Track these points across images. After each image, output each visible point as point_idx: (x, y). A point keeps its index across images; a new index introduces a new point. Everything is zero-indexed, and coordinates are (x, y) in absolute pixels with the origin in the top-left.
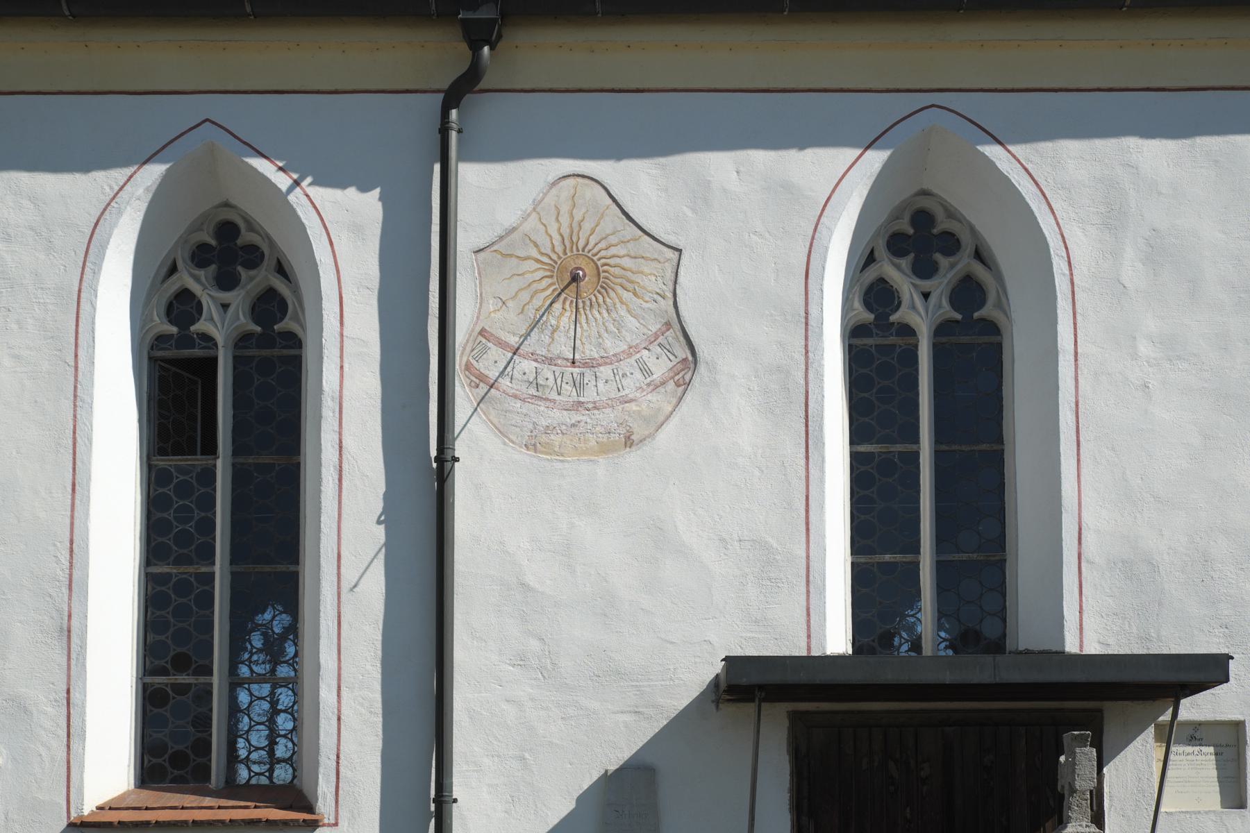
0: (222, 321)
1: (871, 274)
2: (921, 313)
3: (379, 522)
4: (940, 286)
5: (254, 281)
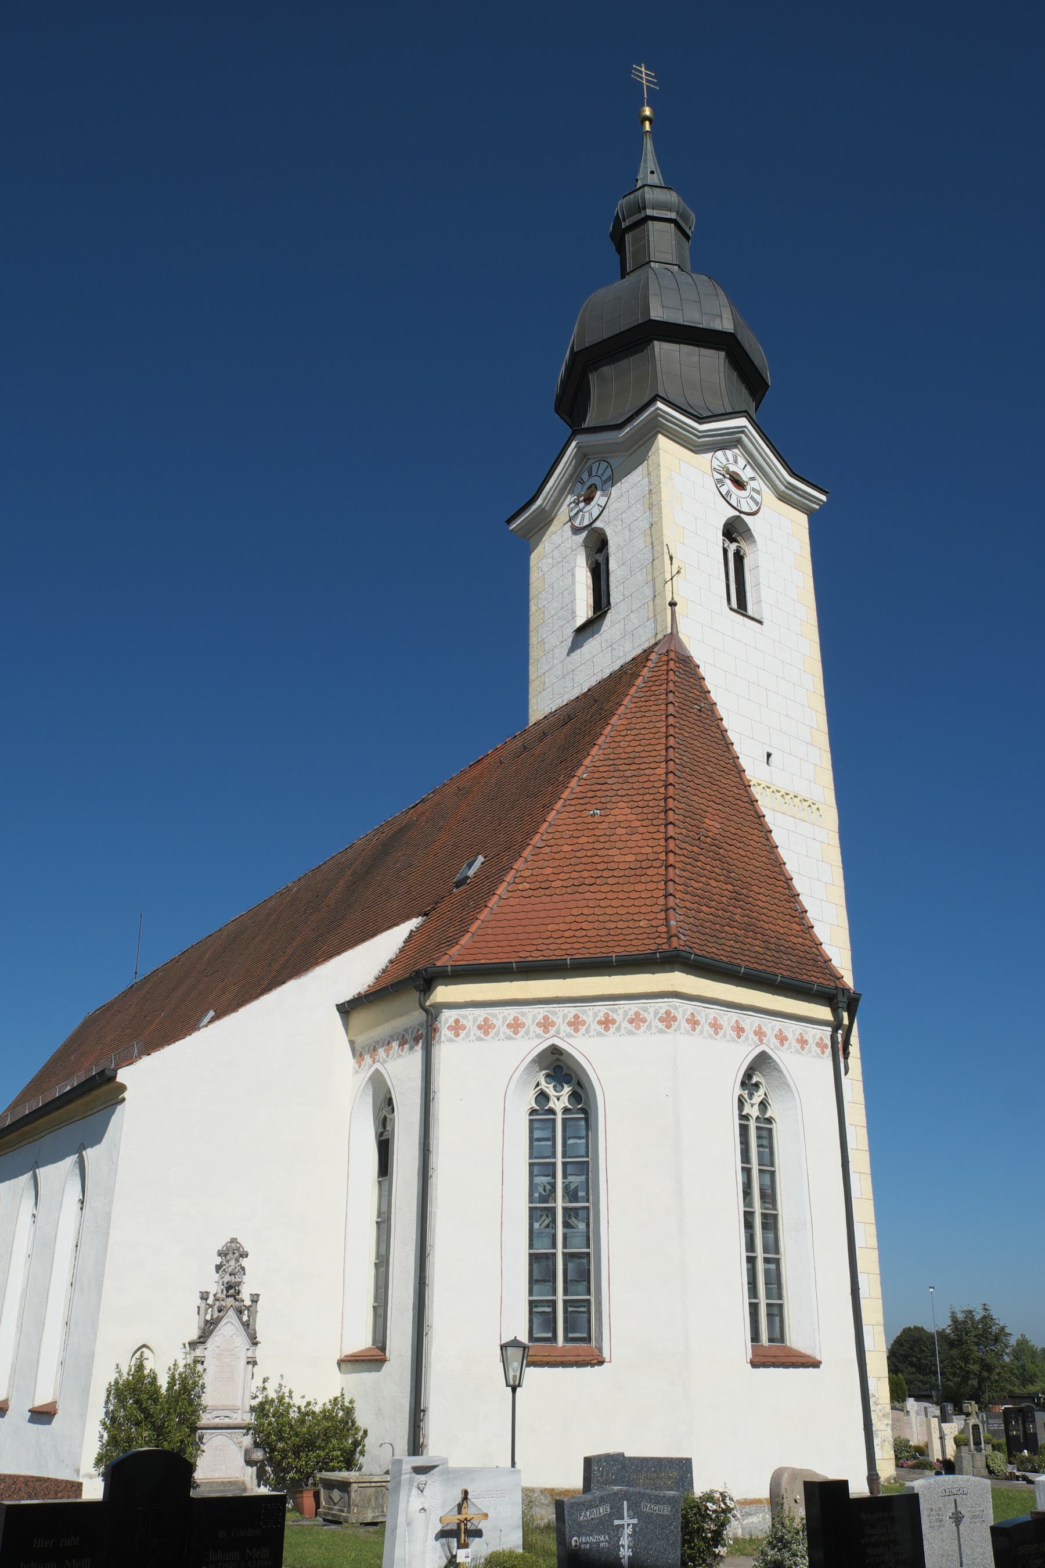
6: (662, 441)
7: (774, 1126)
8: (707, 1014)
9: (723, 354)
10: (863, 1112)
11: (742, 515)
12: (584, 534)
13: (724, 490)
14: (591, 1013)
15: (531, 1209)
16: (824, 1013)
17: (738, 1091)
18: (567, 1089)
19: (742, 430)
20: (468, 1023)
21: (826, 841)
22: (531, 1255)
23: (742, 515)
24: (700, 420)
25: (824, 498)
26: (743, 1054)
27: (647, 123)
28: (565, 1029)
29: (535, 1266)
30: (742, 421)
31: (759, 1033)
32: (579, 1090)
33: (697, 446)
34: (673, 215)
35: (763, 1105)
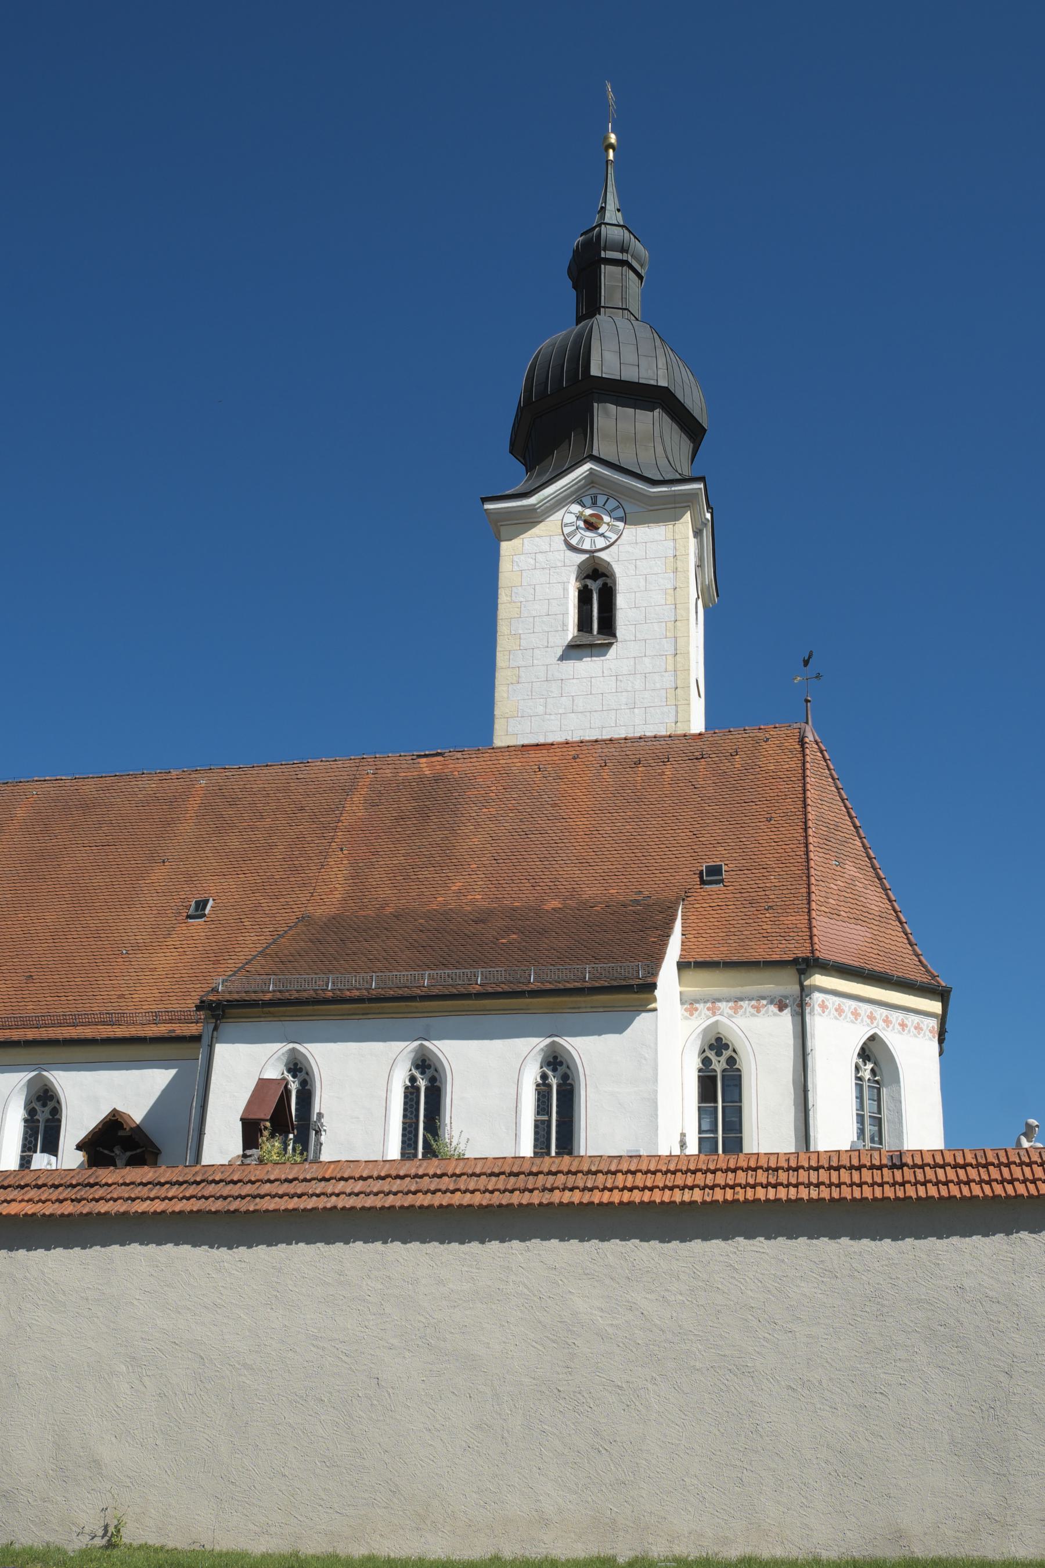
0: (719, 1065)
1: (704, 1055)
2: (422, 1084)
3: (79, 1147)
4: (723, 1059)
5: (726, 1054)
8: (913, 1019)
12: (584, 557)
17: (855, 1059)
18: (870, 1066)
28: (882, 1024)
31: (872, 1018)
32: (876, 1069)
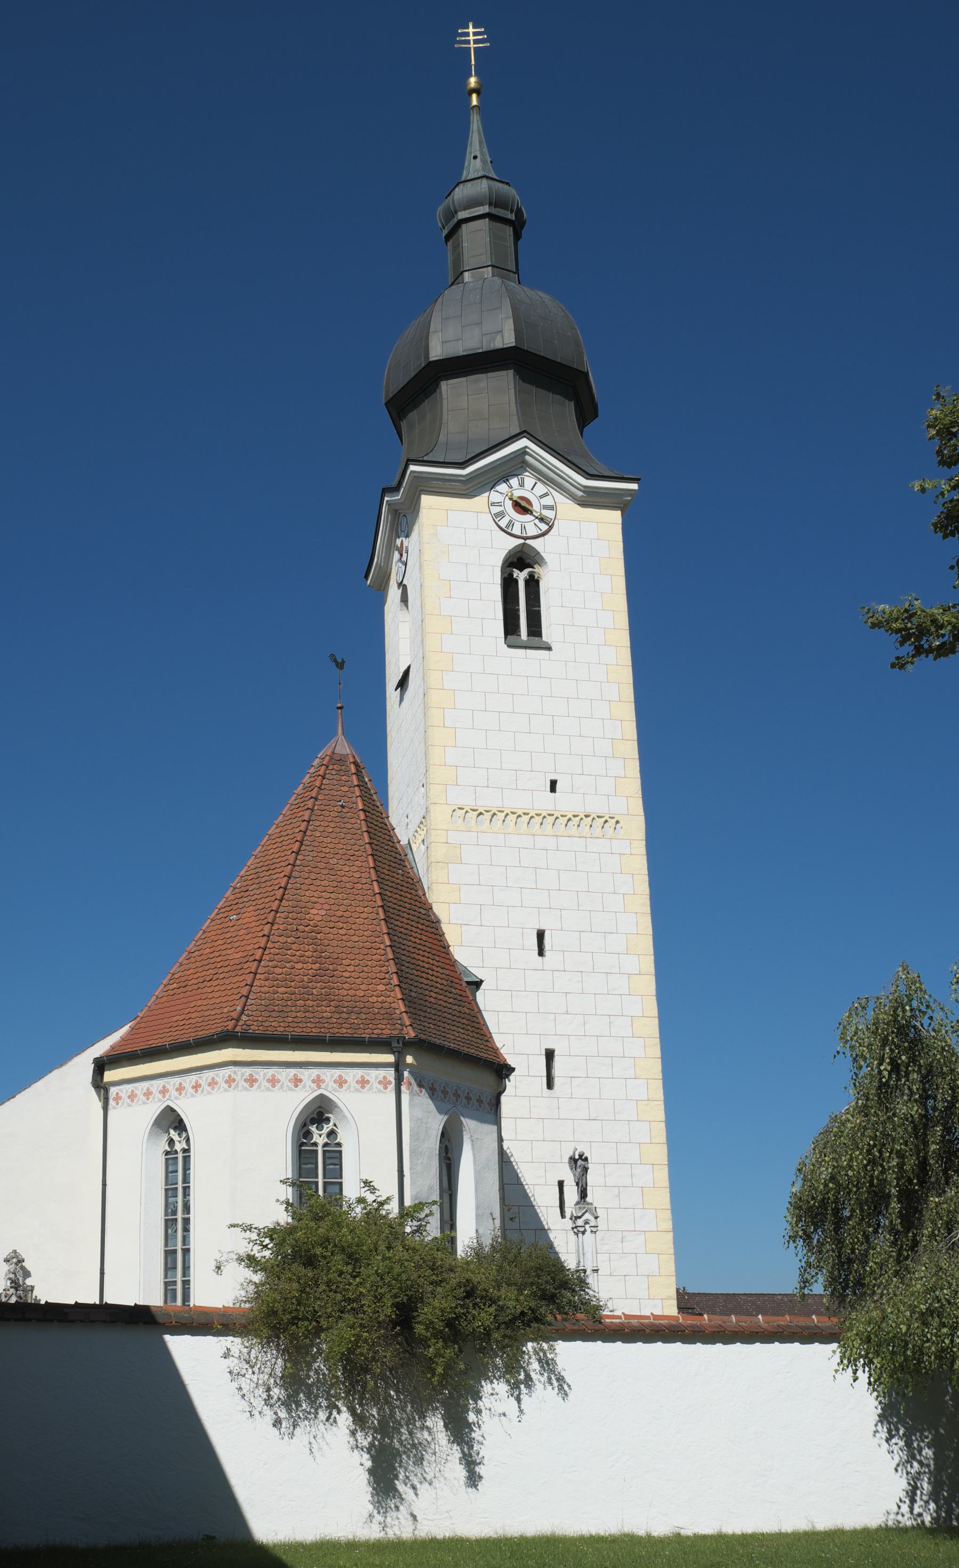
6: (427, 501)
7: (343, 1149)
8: (262, 1074)
9: (511, 372)
10: (663, 1107)
11: (528, 542)
13: (503, 523)
14: (188, 1081)
15: (166, 1220)
16: (390, 1058)
19: (523, 452)
20: (138, 1092)
21: (627, 851)
22: (166, 1252)
23: (528, 542)
24: (462, 465)
25: (634, 486)
26: (291, 1102)
27: (474, 96)
29: (169, 1259)
30: (523, 442)
33: (468, 489)
34: (485, 209)
35: (332, 1134)
